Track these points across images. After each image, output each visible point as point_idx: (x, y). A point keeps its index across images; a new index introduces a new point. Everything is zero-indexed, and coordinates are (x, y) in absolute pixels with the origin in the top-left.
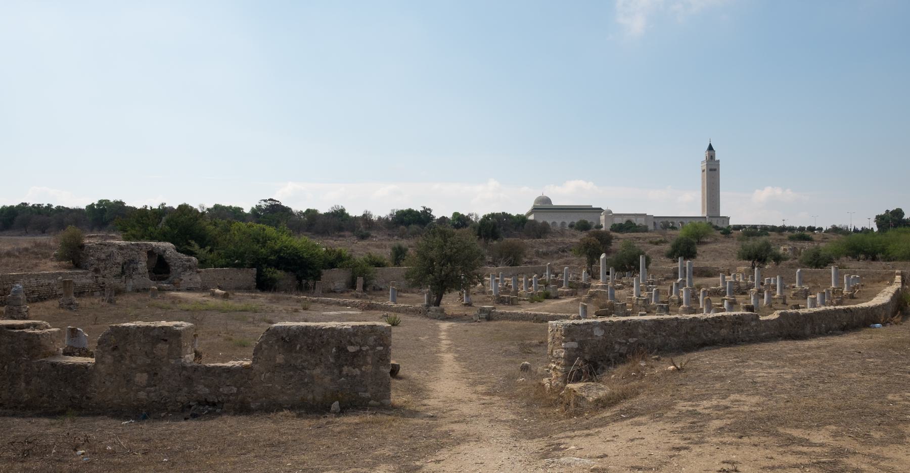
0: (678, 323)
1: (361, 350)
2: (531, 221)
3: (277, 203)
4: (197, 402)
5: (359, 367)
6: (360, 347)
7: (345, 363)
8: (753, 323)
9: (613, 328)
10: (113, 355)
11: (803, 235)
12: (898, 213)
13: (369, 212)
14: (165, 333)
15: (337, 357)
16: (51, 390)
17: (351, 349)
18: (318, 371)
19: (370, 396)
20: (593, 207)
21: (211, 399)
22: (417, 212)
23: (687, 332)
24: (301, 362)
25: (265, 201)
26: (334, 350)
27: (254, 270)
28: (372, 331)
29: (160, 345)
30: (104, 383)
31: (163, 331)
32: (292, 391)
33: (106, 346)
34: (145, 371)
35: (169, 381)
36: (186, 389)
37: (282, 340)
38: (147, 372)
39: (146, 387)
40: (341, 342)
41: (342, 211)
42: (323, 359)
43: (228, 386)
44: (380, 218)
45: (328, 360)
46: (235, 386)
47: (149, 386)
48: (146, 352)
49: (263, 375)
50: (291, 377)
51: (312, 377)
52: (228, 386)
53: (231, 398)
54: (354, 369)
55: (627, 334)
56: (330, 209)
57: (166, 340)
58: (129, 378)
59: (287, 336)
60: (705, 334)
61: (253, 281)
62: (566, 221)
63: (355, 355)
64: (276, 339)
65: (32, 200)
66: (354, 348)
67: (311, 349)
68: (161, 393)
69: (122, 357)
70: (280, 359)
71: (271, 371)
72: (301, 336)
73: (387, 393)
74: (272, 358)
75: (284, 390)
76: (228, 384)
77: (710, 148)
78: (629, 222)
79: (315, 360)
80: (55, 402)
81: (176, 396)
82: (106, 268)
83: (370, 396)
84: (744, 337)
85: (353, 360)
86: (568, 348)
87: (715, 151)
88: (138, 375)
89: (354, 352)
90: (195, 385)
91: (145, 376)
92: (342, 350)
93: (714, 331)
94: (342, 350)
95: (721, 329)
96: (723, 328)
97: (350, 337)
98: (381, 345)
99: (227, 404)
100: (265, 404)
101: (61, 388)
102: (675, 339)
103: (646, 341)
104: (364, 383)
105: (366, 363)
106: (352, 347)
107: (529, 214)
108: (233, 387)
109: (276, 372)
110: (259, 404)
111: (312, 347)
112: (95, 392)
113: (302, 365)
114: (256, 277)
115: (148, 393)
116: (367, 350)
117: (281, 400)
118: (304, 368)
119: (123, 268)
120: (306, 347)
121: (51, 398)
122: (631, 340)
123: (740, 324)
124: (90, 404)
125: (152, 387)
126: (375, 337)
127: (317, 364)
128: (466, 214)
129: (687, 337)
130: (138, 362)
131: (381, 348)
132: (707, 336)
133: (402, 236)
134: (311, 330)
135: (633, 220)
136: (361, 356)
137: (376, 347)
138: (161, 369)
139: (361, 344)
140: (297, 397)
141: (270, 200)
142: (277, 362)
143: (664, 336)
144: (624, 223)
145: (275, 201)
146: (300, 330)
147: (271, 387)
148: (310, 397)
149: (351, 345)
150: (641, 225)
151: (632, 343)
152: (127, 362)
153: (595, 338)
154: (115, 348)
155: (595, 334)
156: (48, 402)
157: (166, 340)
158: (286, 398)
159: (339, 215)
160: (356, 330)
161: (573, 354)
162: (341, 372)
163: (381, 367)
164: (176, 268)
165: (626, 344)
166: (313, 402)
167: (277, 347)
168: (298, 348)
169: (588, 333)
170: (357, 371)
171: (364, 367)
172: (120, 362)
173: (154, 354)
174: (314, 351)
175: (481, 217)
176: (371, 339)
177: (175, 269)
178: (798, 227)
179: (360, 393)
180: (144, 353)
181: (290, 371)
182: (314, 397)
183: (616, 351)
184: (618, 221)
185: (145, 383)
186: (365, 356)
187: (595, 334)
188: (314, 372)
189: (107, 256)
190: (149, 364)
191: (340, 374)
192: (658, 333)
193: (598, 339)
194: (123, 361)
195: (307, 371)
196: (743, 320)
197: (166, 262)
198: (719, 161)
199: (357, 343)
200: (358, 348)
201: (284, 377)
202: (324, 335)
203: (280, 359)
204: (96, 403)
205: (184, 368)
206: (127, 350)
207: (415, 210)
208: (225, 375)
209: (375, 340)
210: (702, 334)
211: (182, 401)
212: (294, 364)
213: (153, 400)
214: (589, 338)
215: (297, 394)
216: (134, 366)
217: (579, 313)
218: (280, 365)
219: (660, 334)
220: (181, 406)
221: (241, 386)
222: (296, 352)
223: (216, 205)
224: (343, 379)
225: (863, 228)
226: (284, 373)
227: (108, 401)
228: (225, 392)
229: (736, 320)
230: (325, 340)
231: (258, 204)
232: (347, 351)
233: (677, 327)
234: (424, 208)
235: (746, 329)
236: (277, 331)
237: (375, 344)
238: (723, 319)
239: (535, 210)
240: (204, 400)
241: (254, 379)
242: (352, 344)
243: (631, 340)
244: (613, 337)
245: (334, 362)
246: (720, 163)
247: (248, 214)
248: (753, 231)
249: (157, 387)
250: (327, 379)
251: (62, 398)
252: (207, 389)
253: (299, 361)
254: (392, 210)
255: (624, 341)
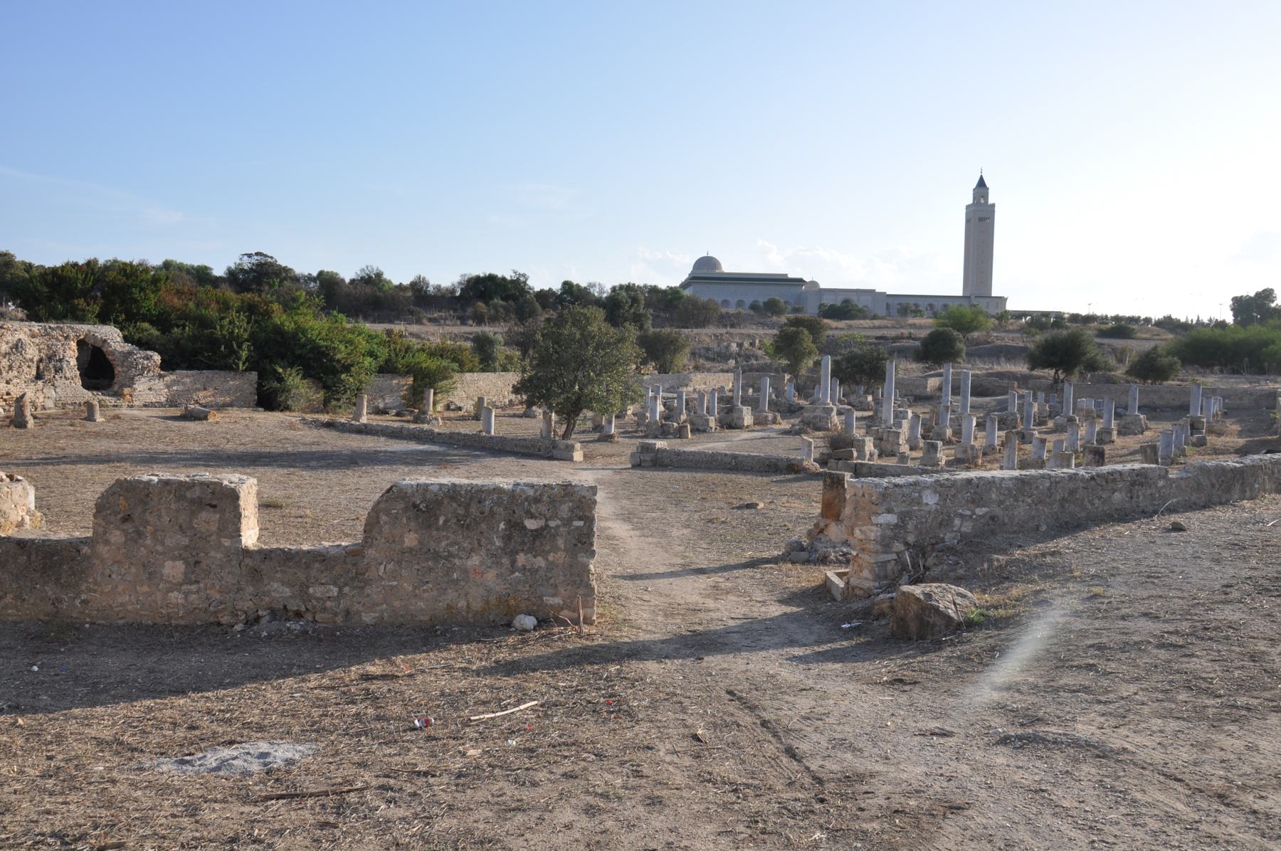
0: (1051, 483)
1: (547, 526)
2: (689, 299)
3: (269, 260)
4: (268, 611)
5: (544, 554)
6: (547, 520)
7: (520, 548)
8: (1161, 483)
9: (953, 491)
10: (124, 530)
11: (1122, 328)
12: (1267, 295)
13: (424, 279)
14: (213, 493)
15: (507, 538)
16: (19, 587)
17: (531, 524)
18: (475, 560)
19: (561, 603)
20: (791, 276)
21: (293, 606)
22: (504, 279)
23: (1063, 499)
24: (447, 545)
25: (250, 256)
26: (502, 526)
27: (254, 376)
28: (566, 495)
29: (204, 515)
30: (110, 576)
31: (210, 491)
32: (432, 593)
33: (110, 514)
34: (180, 557)
35: (222, 574)
36: (251, 589)
37: (415, 507)
38: (183, 559)
39: (181, 585)
40: (514, 512)
41: (379, 275)
42: (483, 541)
43: (322, 584)
44: (438, 288)
45: (493, 544)
46: (335, 584)
47: (187, 583)
48: (181, 527)
49: (382, 567)
50: (430, 569)
51: (465, 571)
52: (322, 584)
53: (329, 604)
54: (535, 557)
55: (973, 501)
56: (359, 273)
57: (214, 506)
58: (152, 570)
59: (422, 502)
60: (1089, 501)
61: (251, 393)
62: (746, 300)
63: (537, 534)
64: (403, 506)
65: (103, 256)
66: (535, 522)
67: (464, 525)
68: (208, 595)
69: (140, 534)
70: (410, 540)
71: (396, 559)
72: (445, 502)
73: (589, 599)
74: (397, 539)
75: (417, 591)
76: (323, 581)
77: (982, 183)
78: (846, 301)
79: (470, 543)
80: (26, 606)
81: (234, 600)
82: (10, 368)
83: (561, 603)
84: (1146, 506)
85: (534, 543)
86: (881, 525)
87: (988, 189)
88: (169, 564)
89: (536, 530)
90: (266, 582)
91: (180, 566)
92: (515, 526)
93: (1104, 496)
94: (515, 526)
95: (1113, 493)
96: (1116, 491)
97: (530, 504)
98: (580, 519)
99: (321, 615)
100: (385, 614)
101: (37, 584)
102: (1046, 510)
103: (1001, 512)
104: (552, 581)
105: (555, 549)
106: (533, 521)
107: (685, 285)
108: (332, 587)
109: (403, 562)
110: (377, 615)
111: (465, 521)
112: (95, 591)
113: (448, 551)
114: (256, 386)
115: (187, 594)
116: (558, 526)
117: (412, 607)
118: (451, 555)
119: (38, 368)
120: (454, 520)
121: (19, 600)
122: (980, 511)
123: (1141, 484)
124: (87, 611)
125: (191, 584)
126: (571, 504)
127: (472, 550)
128: (583, 284)
129: (1063, 506)
130: (168, 542)
131: (581, 523)
132: (1093, 504)
133: (480, 320)
134: (463, 492)
135: (854, 298)
136: (548, 536)
137: (572, 521)
138: (207, 554)
139: (548, 516)
140: (441, 604)
141: (257, 254)
142: (406, 545)
143: (1029, 505)
144: (839, 304)
145: (266, 256)
146: (444, 492)
147: (396, 586)
148: (462, 604)
149: (532, 518)
150: (865, 309)
151: (980, 516)
152: (148, 542)
153: (924, 508)
154: (127, 519)
155: (925, 501)
156: (16, 607)
157: (214, 506)
158: (421, 604)
159: (372, 281)
160: (538, 493)
161: (889, 533)
162: (513, 562)
163: (579, 555)
164: (125, 369)
165: (971, 517)
166: (468, 613)
167: (404, 520)
168: (441, 522)
169: (913, 499)
170: (540, 562)
171: (552, 554)
172: (136, 542)
173: (195, 529)
174: (468, 527)
175: (608, 288)
176: (564, 510)
177: (124, 372)
178: (315, 274)
179: (545, 598)
180: (177, 527)
181: (428, 560)
182: (468, 604)
183: (955, 529)
184: (828, 301)
185: (180, 577)
186: (555, 536)
187: (925, 501)
188: (469, 563)
189: (11, 348)
190: (186, 547)
191: (512, 566)
192: (1021, 499)
193: (927, 509)
194: (141, 541)
195: (457, 561)
196: (1146, 478)
197: (107, 359)
198: (993, 205)
199: (540, 514)
200: (541, 523)
201: (418, 570)
202: (485, 500)
203: (410, 540)
204: (98, 610)
205: (247, 552)
206: (147, 522)
207: (500, 276)
208: (317, 565)
209: (572, 511)
210: (1086, 500)
211: (245, 608)
212: (434, 550)
213: (194, 606)
214: (914, 508)
215: (441, 599)
216: (160, 548)
217: (857, 458)
218: (411, 550)
219: (1023, 501)
220: (243, 617)
221: (346, 585)
222: (438, 529)
223: (166, 261)
224: (517, 574)
225: (1210, 320)
226: (418, 563)
227: (117, 607)
228: (319, 595)
229: (1136, 478)
230: (487, 510)
231: (238, 262)
232: (524, 527)
233: (1049, 489)
234: (515, 273)
235: (1149, 492)
236: (406, 493)
237: (570, 517)
238: (1117, 476)
239: (693, 279)
240: (281, 607)
241: (367, 574)
242: (532, 516)
243: (980, 511)
244: (951, 505)
245: (502, 545)
246: (996, 209)
247: (220, 277)
248: (1040, 321)
249: (202, 585)
250: (491, 575)
251: (38, 602)
252: (288, 590)
253: (443, 544)
254: (462, 275)
255: (968, 513)
